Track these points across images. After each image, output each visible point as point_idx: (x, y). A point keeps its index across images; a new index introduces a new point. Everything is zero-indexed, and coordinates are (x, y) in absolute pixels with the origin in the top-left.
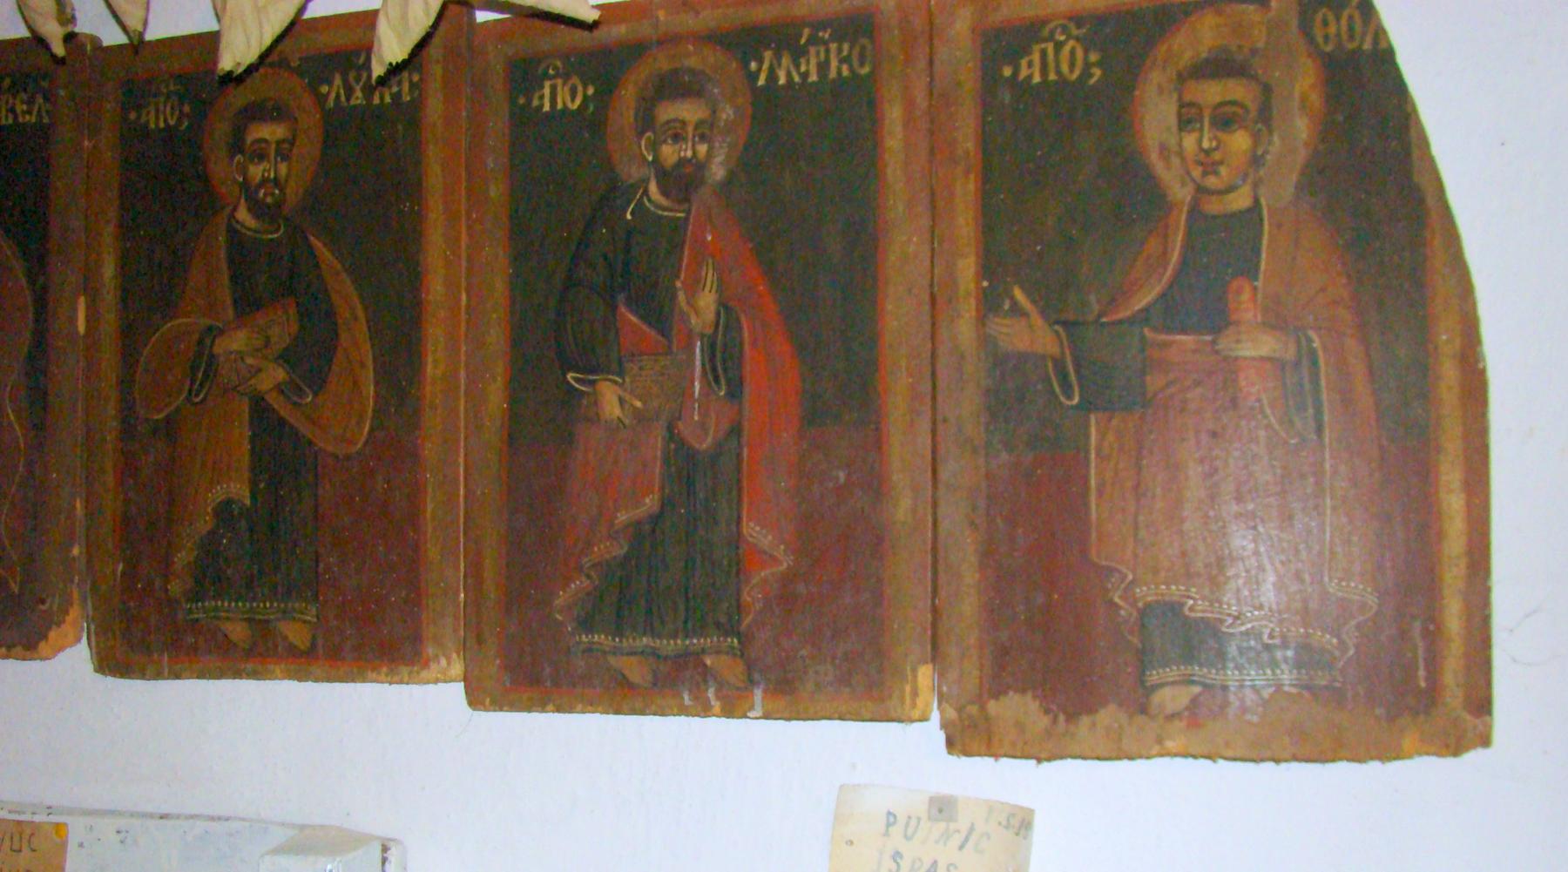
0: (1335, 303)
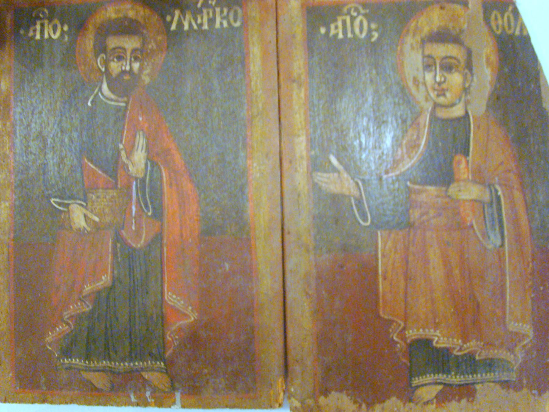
0: (509, 171)
